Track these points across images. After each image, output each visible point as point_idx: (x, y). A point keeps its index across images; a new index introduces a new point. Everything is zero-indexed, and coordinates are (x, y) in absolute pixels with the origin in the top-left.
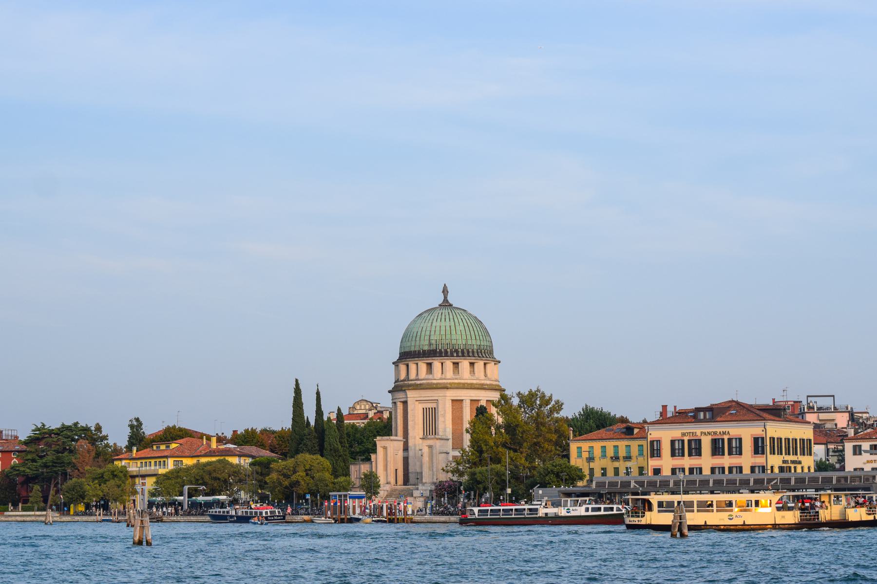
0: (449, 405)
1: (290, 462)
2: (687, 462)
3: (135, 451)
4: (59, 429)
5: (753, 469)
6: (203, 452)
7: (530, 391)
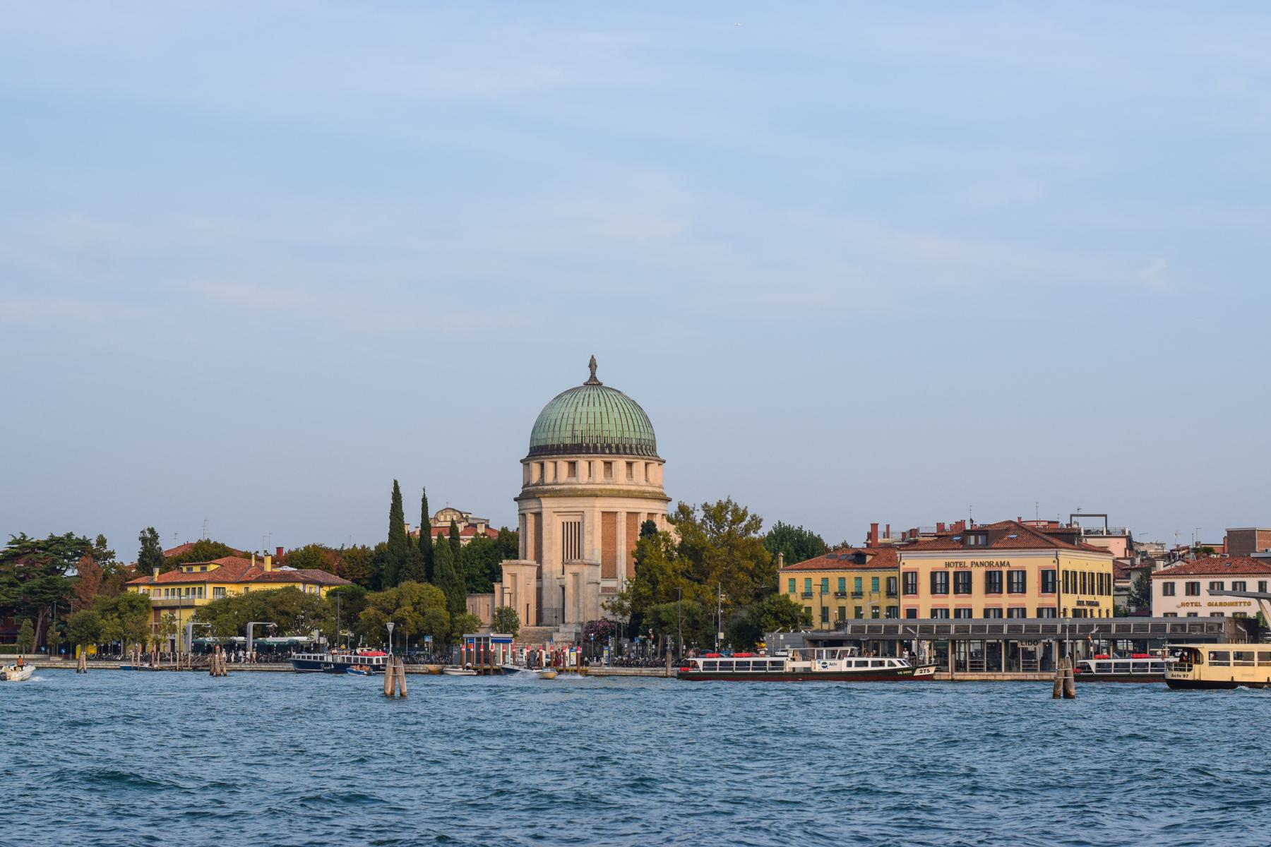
0: (598, 519)
1: (391, 592)
2: (952, 601)
3: (157, 574)
4: (46, 542)
5: (1040, 612)
6: (254, 577)
7: (719, 503)
